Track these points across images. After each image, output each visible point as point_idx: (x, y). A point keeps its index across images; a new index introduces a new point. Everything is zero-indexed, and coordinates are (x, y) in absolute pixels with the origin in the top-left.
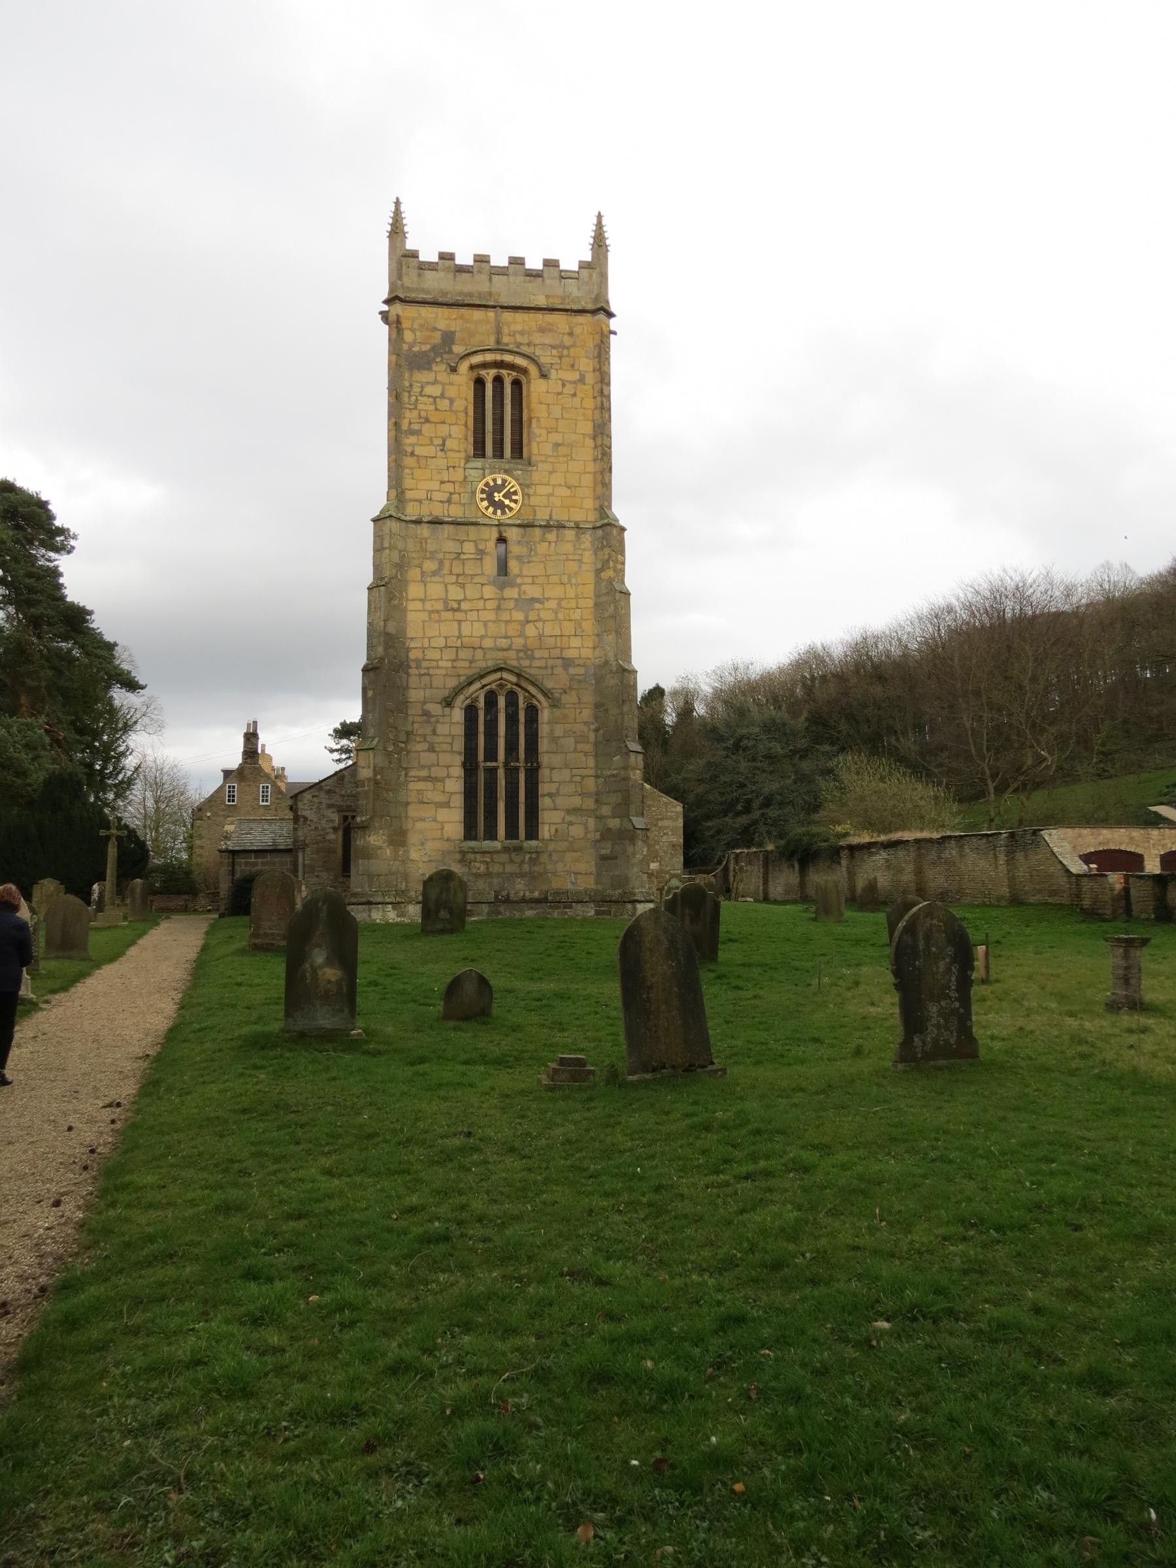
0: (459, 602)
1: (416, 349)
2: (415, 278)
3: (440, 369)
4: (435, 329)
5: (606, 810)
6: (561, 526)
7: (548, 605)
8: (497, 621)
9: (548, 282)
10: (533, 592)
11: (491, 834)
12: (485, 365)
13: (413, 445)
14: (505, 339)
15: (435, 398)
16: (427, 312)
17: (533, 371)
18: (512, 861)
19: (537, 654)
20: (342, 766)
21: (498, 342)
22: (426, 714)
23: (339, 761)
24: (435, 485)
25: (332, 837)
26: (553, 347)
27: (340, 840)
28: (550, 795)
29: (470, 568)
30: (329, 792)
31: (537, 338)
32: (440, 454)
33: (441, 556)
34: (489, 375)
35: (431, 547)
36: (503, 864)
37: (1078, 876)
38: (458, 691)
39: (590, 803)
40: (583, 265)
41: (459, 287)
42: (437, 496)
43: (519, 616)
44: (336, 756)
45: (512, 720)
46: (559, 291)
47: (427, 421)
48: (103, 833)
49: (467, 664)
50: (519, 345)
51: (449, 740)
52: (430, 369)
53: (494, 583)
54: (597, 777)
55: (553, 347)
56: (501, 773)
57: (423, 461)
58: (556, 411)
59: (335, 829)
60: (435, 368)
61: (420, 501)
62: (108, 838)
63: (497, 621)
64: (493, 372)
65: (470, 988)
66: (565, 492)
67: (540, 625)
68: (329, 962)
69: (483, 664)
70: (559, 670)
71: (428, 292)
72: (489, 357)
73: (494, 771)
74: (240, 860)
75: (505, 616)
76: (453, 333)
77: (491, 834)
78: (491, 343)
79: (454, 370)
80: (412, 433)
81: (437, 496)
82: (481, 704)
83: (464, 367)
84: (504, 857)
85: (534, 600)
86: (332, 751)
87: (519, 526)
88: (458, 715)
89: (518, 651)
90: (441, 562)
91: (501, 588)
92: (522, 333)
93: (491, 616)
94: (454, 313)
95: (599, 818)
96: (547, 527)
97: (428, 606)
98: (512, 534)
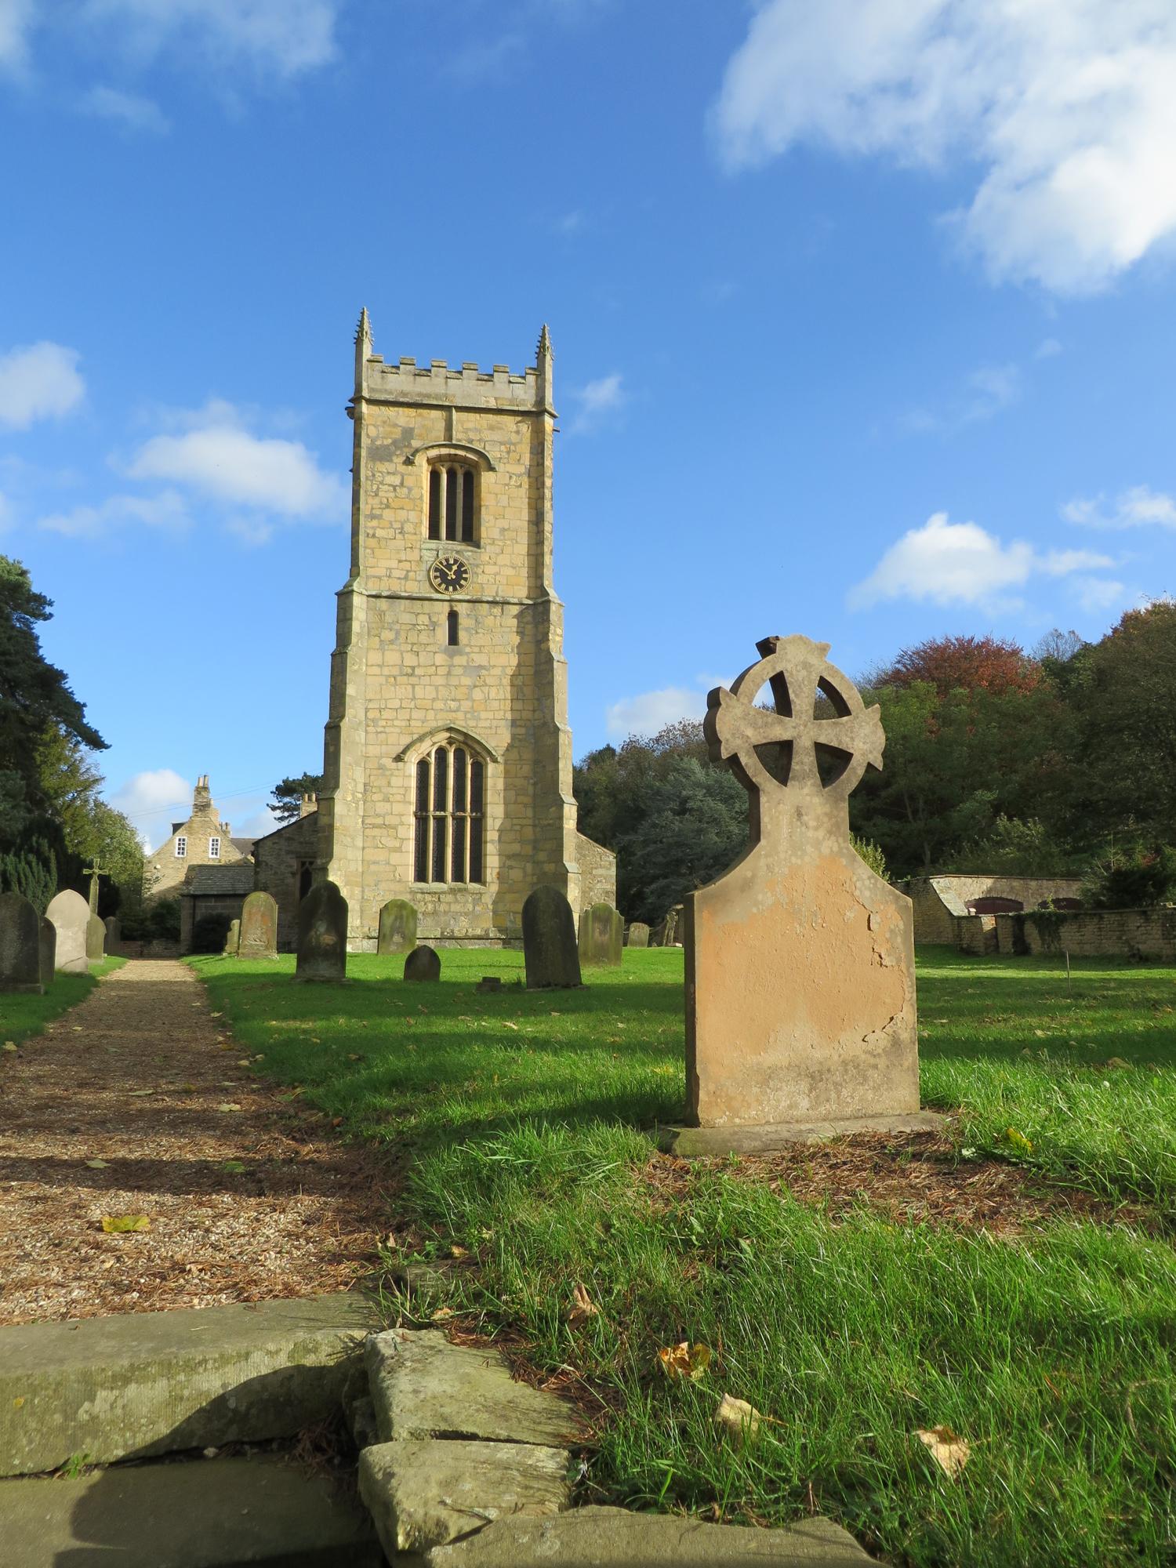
0: (413, 668)
1: (379, 443)
2: (379, 381)
4: (396, 425)
7: (494, 672)
8: (447, 685)
9: (498, 385)
10: (480, 659)
11: (440, 877)
13: (374, 528)
15: (395, 487)
18: (457, 901)
19: (483, 715)
20: (285, 824)
23: (281, 819)
24: (394, 564)
25: (290, 880)
26: (501, 443)
27: (298, 885)
29: (423, 638)
30: (289, 839)
31: (488, 435)
32: (399, 536)
33: (397, 627)
35: (388, 618)
36: (449, 904)
37: (960, 918)
39: (528, 850)
41: (418, 389)
42: (396, 573)
43: (467, 681)
44: (278, 813)
46: (508, 395)
47: (388, 506)
48: (86, 872)
49: (419, 724)
50: (471, 441)
51: (402, 791)
52: (391, 461)
54: (534, 826)
55: (501, 443)
56: (450, 821)
57: (383, 543)
58: (504, 500)
59: (293, 874)
60: (395, 459)
61: (380, 578)
62: (90, 876)
63: (447, 685)
65: (424, 959)
67: (486, 689)
68: (328, 931)
71: (391, 393)
74: (201, 904)
75: (454, 681)
76: (412, 429)
77: (440, 877)
79: (409, 462)
80: (373, 517)
81: (396, 573)
82: (432, 760)
84: (450, 898)
85: (481, 667)
86: (274, 808)
87: (468, 601)
88: (413, 770)
89: (466, 713)
90: (398, 633)
91: (451, 656)
92: (476, 430)
94: (412, 412)
95: (536, 863)
96: (494, 603)
97: (386, 671)
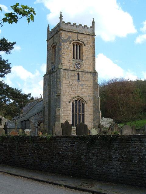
3: (68, 43)
5: (95, 122)
6: (88, 72)
10: (83, 83)
12: (75, 43)
14: (79, 38)
16: (66, 33)
17: (83, 45)
21: (77, 35)
22: (66, 104)
28: (86, 119)
29: (73, 78)
34: (75, 44)
38: (71, 100)
40: (91, 27)
43: (81, 87)
45: (80, 106)
53: (77, 81)
57: (65, 59)
64: (76, 44)
66: (88, 66)
69: (75, 95)
70: (87, 97)
72: (76, 41)
73: (76, 114)
78: (76, 39)
79: (70, 43)
80: (63, 53)
83: (72, 43)
93: (77, 87)
96: (85, 72)
98: (80, 73)
